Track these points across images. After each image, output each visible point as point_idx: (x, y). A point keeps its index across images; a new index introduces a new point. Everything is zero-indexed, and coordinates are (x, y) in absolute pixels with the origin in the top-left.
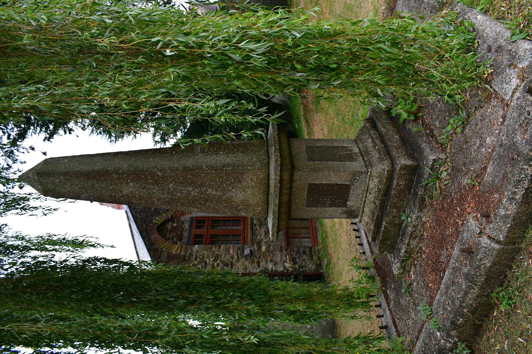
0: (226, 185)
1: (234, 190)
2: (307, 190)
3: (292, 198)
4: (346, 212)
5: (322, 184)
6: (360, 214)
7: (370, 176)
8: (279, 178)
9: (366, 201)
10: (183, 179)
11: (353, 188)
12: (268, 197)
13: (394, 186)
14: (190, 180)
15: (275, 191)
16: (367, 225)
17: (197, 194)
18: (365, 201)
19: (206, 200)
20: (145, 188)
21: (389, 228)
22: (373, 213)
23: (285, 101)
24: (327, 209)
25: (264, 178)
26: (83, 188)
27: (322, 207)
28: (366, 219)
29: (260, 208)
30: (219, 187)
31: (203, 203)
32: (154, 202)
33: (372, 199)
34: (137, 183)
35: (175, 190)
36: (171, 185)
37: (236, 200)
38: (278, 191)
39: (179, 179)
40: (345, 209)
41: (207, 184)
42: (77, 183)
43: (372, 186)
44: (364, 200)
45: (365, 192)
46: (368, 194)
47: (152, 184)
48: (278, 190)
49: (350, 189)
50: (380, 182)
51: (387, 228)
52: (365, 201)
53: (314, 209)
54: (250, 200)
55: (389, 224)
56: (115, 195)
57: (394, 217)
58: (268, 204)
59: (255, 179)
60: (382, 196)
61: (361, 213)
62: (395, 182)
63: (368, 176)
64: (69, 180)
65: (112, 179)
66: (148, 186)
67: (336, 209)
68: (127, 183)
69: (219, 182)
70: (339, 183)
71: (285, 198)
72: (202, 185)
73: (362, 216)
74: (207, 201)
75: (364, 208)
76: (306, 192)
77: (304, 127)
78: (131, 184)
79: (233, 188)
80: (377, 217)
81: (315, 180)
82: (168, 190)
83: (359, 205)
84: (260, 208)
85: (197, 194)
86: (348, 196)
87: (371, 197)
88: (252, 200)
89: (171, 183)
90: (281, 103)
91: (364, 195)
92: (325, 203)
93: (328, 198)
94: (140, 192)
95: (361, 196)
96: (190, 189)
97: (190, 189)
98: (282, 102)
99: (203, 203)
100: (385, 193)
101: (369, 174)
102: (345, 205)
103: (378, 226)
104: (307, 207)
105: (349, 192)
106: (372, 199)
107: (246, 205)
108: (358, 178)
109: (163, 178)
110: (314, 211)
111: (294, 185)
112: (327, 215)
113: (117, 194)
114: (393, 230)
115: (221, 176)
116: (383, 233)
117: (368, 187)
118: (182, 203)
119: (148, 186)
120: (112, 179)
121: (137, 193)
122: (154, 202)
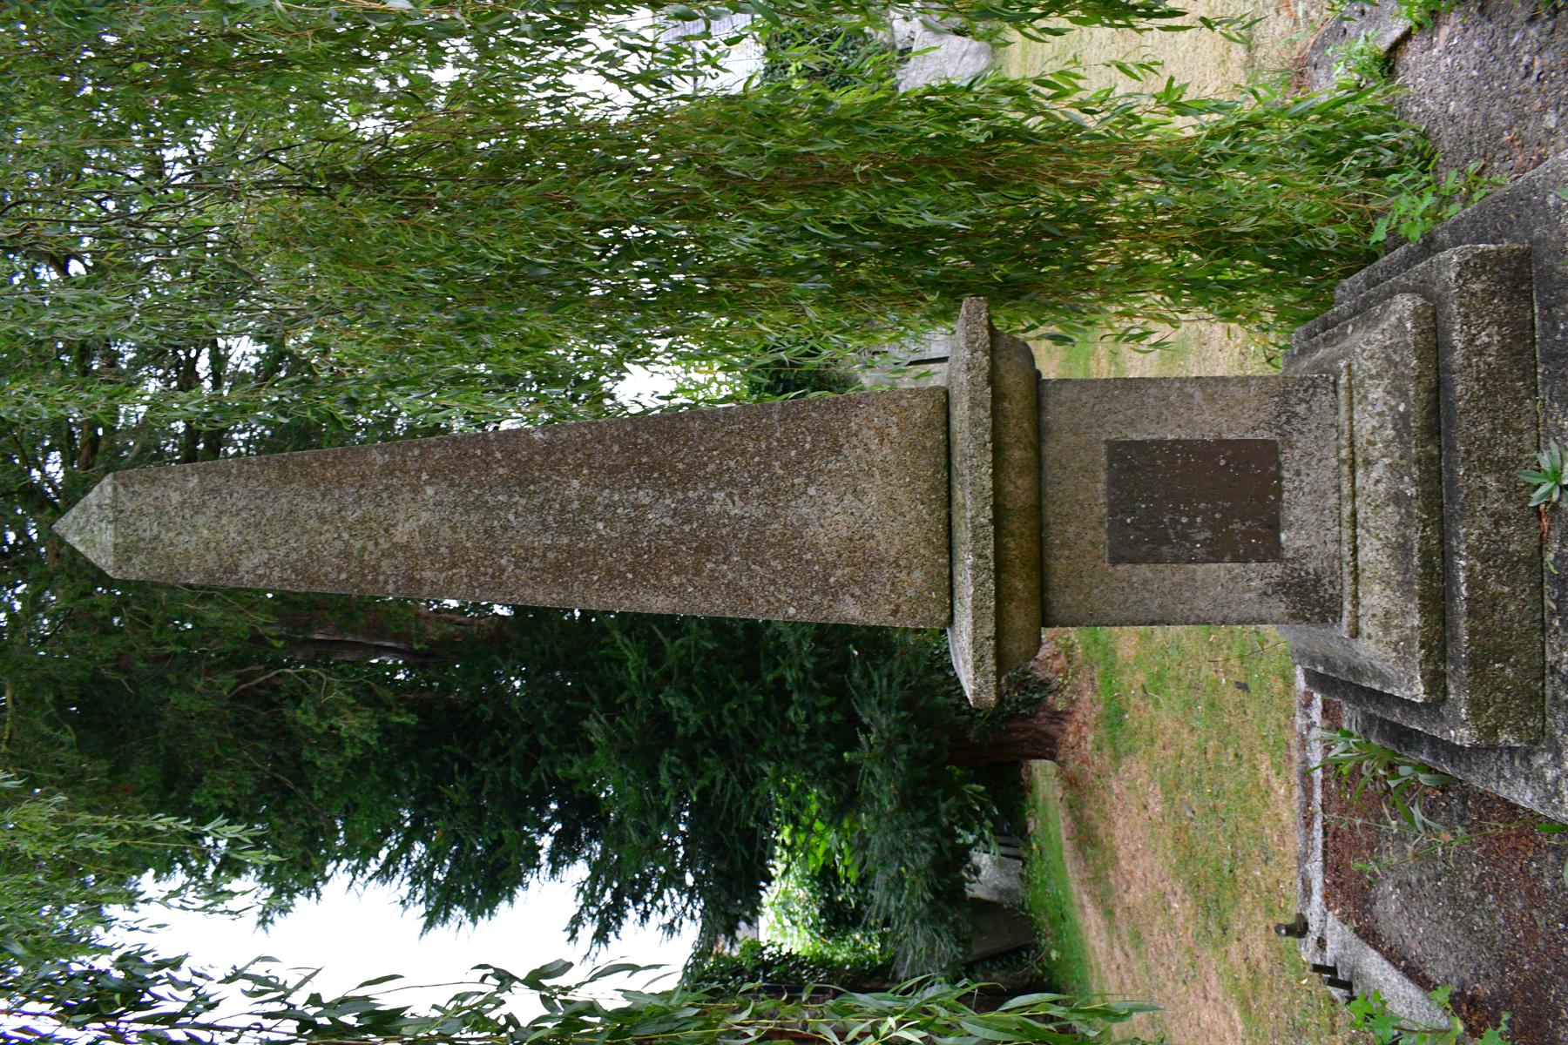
0: (784, 466)
1: (812, 491)
2: (1103, 476)
3: (1044, 502)
4: (1282, 584)
5: (1161, 443)
6: (1348, 589)
7: (1350, 388)
8: (985, 360)
9: (1361, 516)
10: (623, 449)
11: (1290, 459)
12: (949, 516)
13: (1458, 358)
14: (647, 452)
15: (975, 424)
16: (1386, 628)
17: (668, 521)
18: (1354, 514)
19: (706, 550)
20: (479, 505)
21: (1493, 586)
22: (1401, 549)
23: (1008, 892)
24: (1200, 569)
25: (929, 424)
26: (258, 525)
27: (1176, 560)
28: (1376, 598)
29: (917, 575)
30: (756, 479)
31: (689, 561)
32: (502, 570)
33: (1381, 487)
34: (452, 485)
35: (587, 504)
36: (575, 483)
37: (823, 540)
38: (988, 422)
39: (607, 453)
40: (1275, 570)
41: (711, 467)
42: (241, 504)
43: (1365, 423)
44: (1347, 510)
45: (1345, 469)
46: (1360, 472)
47: (505, 482)
48: (984, 415)
49: (1279, 466)
50: (1397, 391)
51: (1482, 585)
52: (1354, 514)
53: (1145, 570)
54: (880, 537)
55: (1484, 560)
56: (364, 548)
57: (1498, 519)
58: (950, 548)
59: (894, 431)
60: (1422, 444)
61: (1348, 580)
62: (1457, 339)
63: (1342, 393)
64: (216, 491)
65: (363, 477)
66: (487, 497)
67: (1237, 568)
68: (416, 490)
69: (758, 453)
70: (1231, 436)
71: (1019, 488)
72: (687, 479)
73: (1356, 602)
74: (708, 552)
75: (1355, 551)
76: (1101, 486)
77: (1074, 887)
78: (430, 491)
79: (810, 481)
80: (1426, 555)
81: (1132, 424)
82: (563, 510)
83: (1332, 548)
84: (917, 575)
85: (668, 521)
86: (1279, 498)
87: (1374, 481)
88: (886, 542)
89: (576, 476)
90: (995, 898)
91: (1346, 489)
92: (1187, 537)
93: (1198, 512)
94: (453, 528)
95: (1333, 501)
96: (644, 497)
97: (644, 497)
98: (1001, 892)
99: (689, 561)
100: (1434, 419)
101: (1343, 381)
102: (1273, 551)
103: (1436, 603)
104: (1116, 560)
105: (1280, 479)
106: (1381, 487)
107: (860, 557)
108: (1301, 409)
109: (549, 454)
110: (1145, 582)
111: (1051, 450)
112: (1203, 604)
113: (370, 545)
114: (1513, 595)
115: (766, 427)
116: (1471, 613)
117: (1352, 445)
118: (609, 571)
119: (487, 497)
120: (363, 477)
121: (445, 531)
122: (502, 570)
